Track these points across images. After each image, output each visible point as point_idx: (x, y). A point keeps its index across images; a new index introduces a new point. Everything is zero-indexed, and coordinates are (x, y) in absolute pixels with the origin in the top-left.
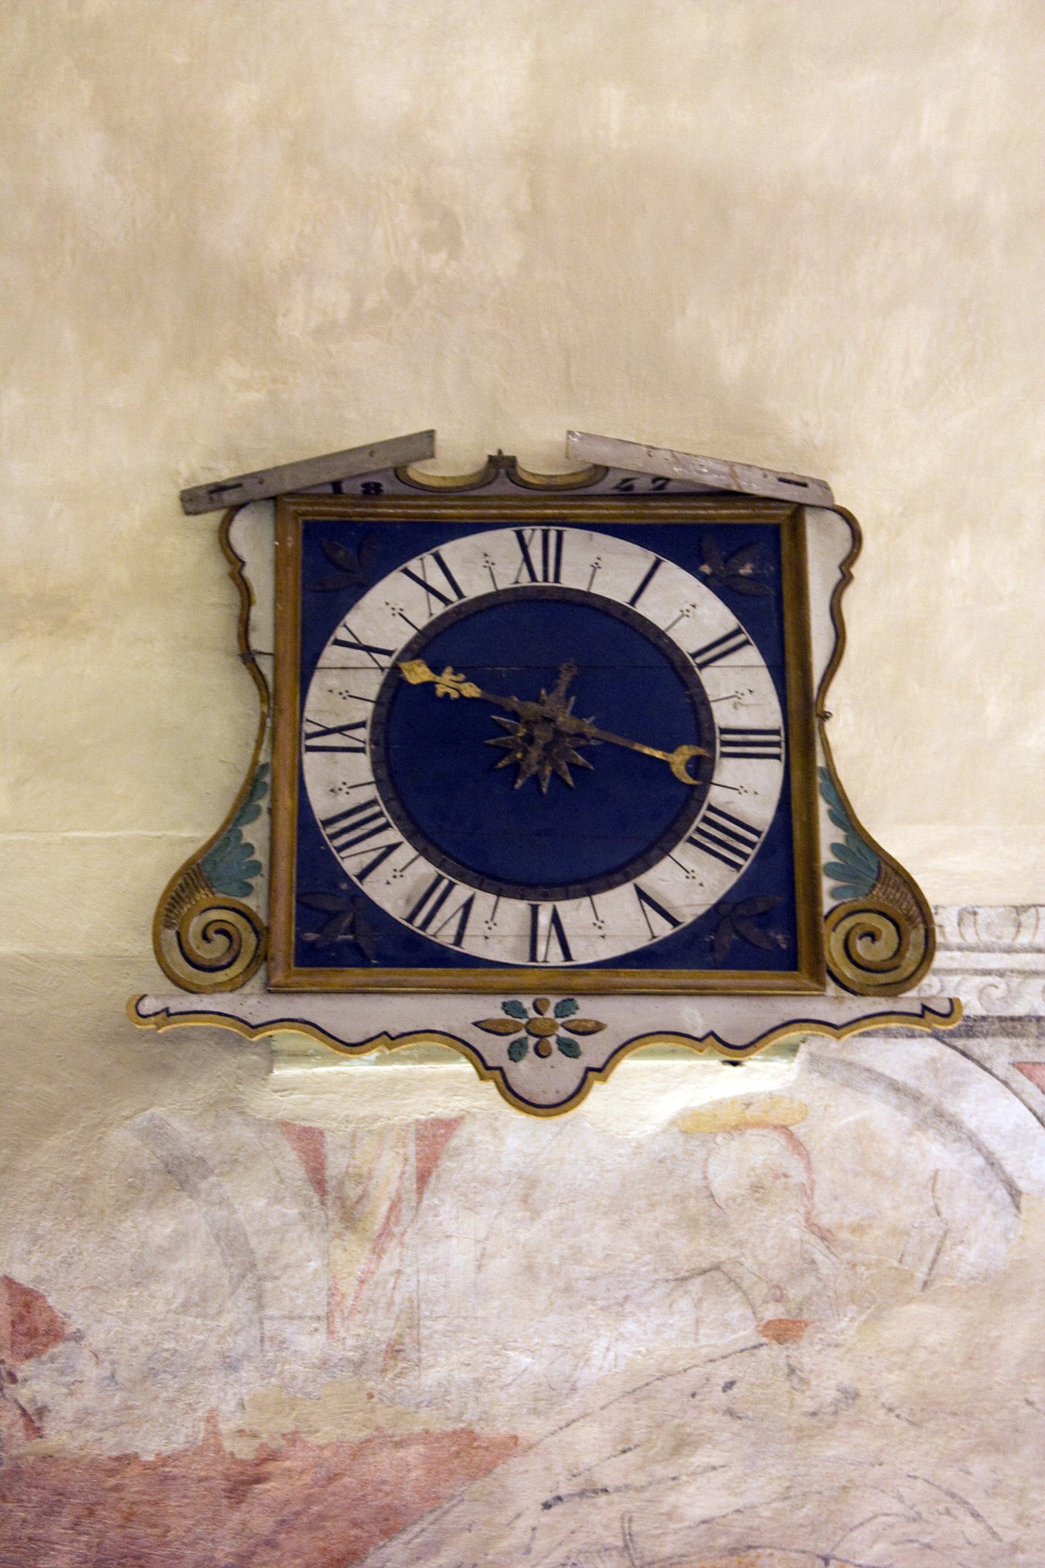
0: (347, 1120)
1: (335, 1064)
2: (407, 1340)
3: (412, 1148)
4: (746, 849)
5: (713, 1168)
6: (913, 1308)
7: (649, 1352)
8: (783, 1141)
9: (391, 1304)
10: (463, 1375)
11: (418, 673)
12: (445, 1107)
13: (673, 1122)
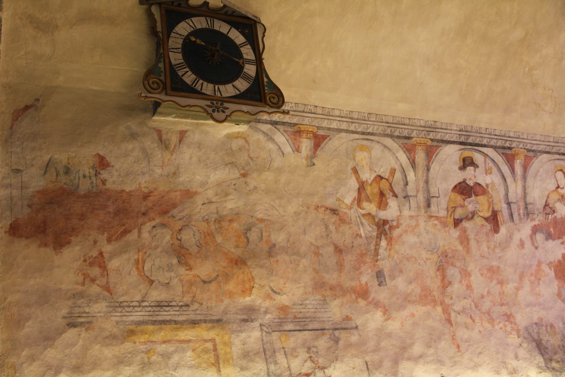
0: (166, 129)
1: (165, 117)
2: (177, 172)
3: (178, 135)
4: (251, 80)
5: (232, 145)
6: (266, 173)
7: (221, 177)
8: (244, 141)
9: (174, 165)
10: (187, 179)
11: (193, 39)
12: (184, 128)
13: (225, 135)
